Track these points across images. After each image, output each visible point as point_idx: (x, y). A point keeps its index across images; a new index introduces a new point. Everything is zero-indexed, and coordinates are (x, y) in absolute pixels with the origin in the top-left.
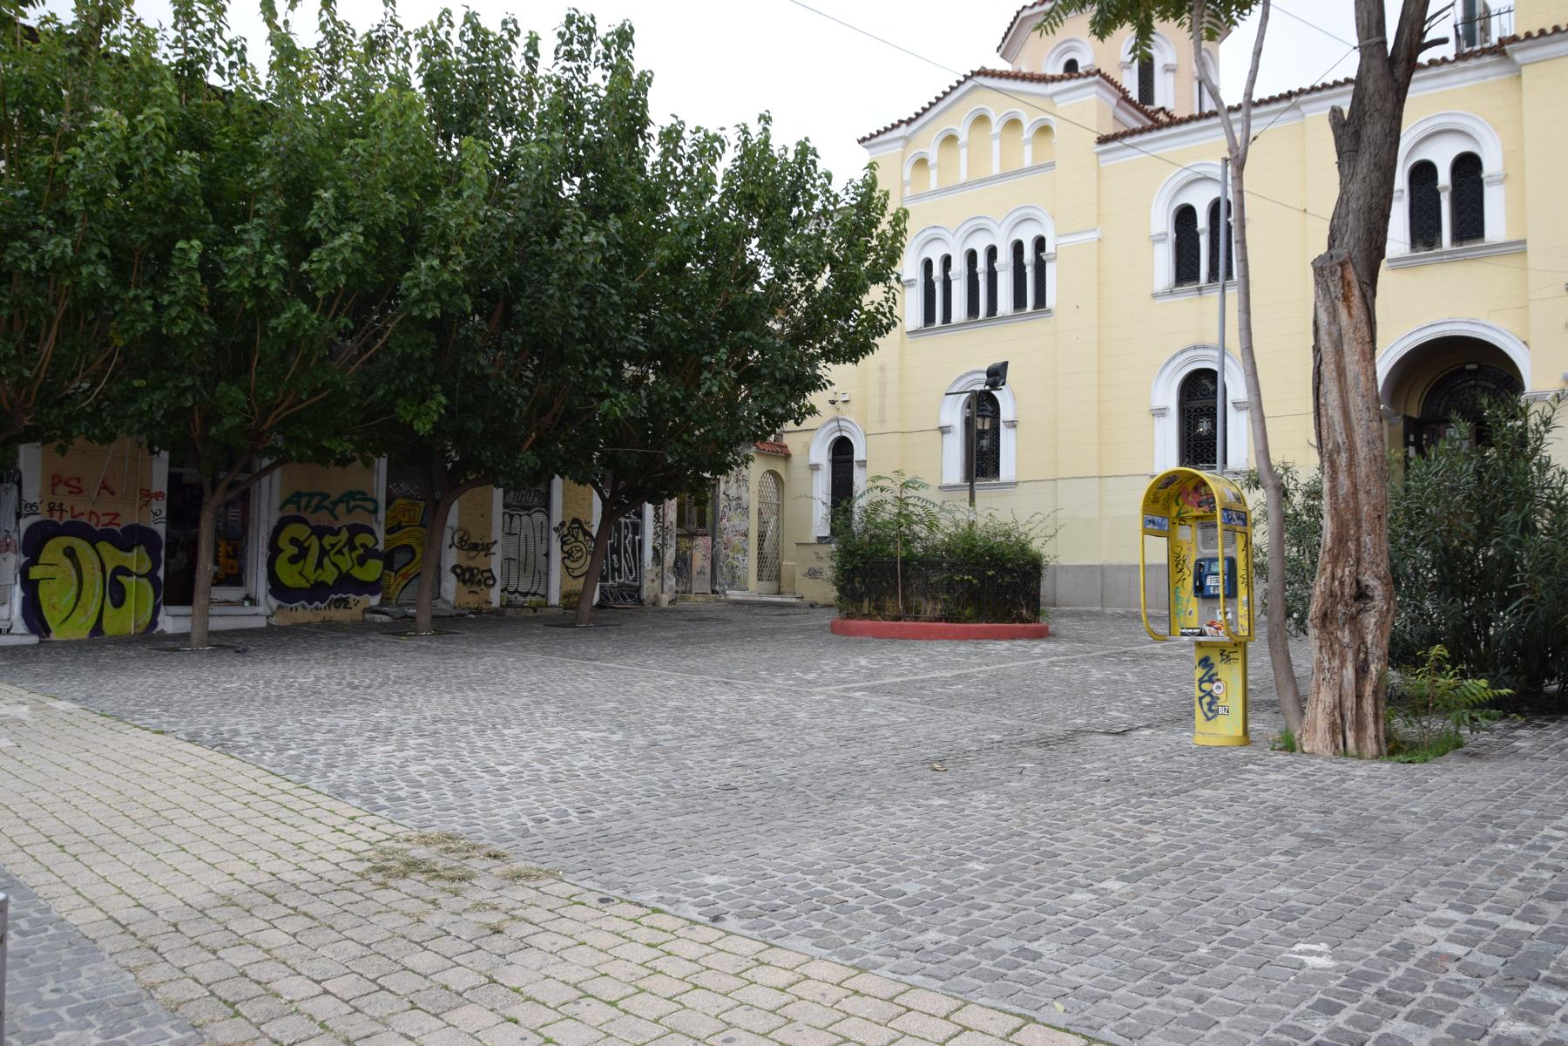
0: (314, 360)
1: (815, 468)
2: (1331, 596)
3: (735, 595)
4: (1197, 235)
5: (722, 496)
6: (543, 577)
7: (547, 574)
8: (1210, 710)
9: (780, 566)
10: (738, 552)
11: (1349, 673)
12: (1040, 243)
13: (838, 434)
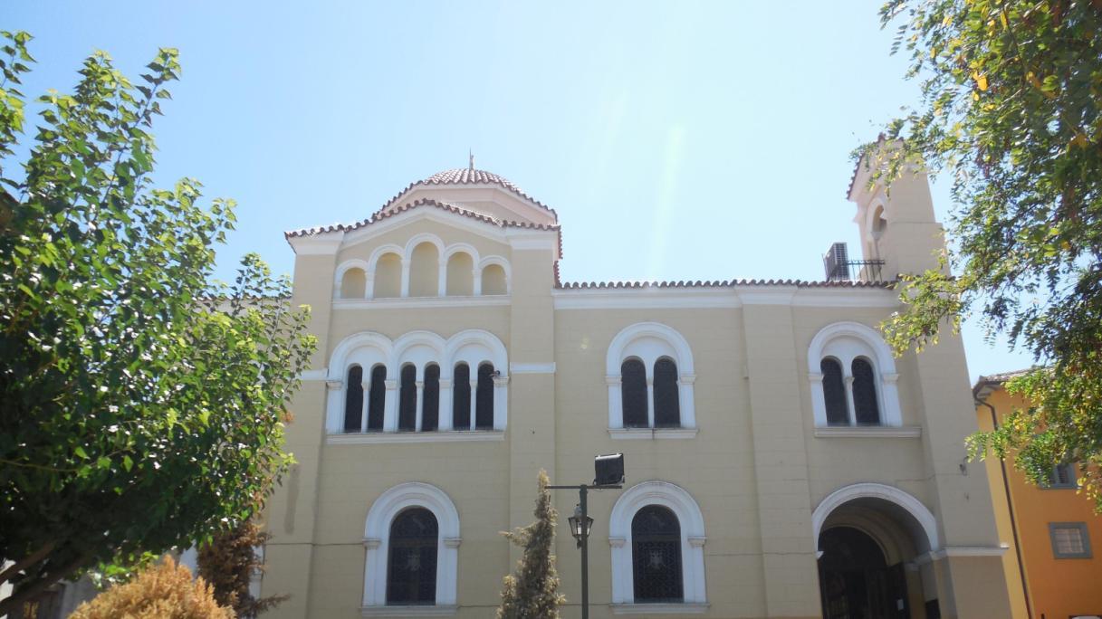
4: (645, 386)
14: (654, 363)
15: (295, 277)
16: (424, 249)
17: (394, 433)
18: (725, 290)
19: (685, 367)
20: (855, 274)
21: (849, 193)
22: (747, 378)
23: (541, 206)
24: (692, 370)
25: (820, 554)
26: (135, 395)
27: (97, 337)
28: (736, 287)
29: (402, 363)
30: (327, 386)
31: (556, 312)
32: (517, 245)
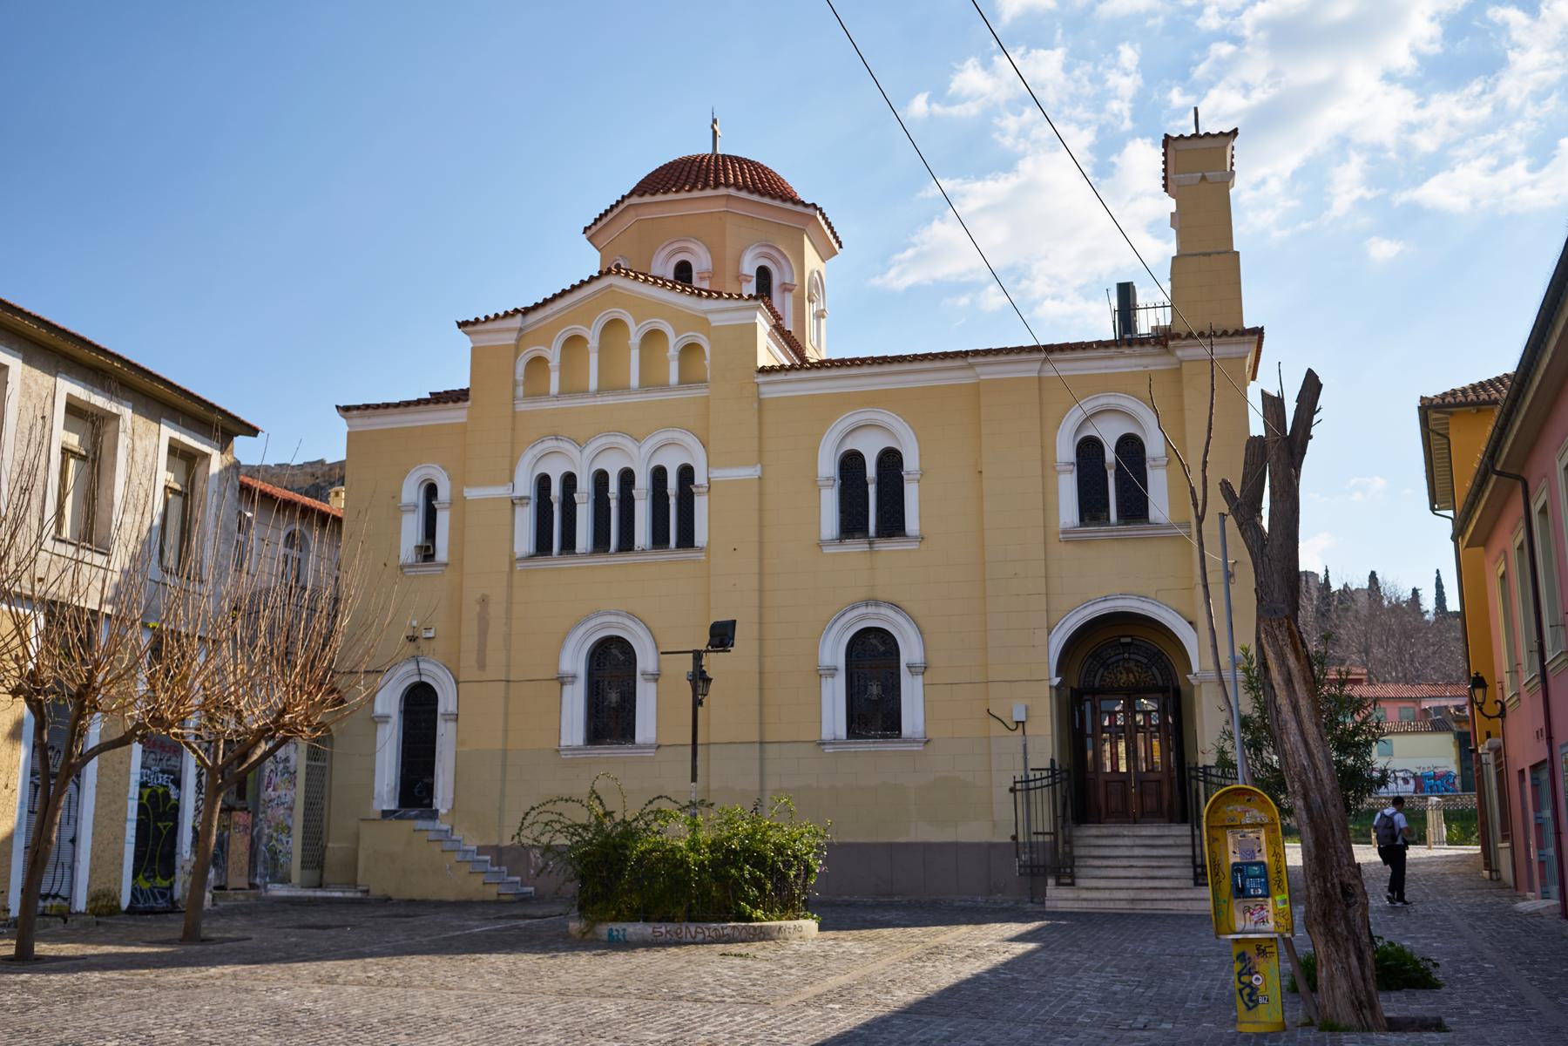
1: (385, 719)
2: (1326, 896)
3: (278, 891)
4: (866, 485)
6: (67, 871)
7: (72, 868)
8: (1251, 1000)
9: (324, 848)
11: (1354, 961)
12: (686, 473)
13: (416, 679)
14: (1115, 441)
16: (614, 325)
17: (531, 557)
19: (911, 463)
20: (1145, 323)
21: (1165, 186)
22: (981, 472)
23: (597, 278)
24: (917, 468)
25: (1056, 681)
27: (87, 467)
29: (593, 470)
32: (717, 320)
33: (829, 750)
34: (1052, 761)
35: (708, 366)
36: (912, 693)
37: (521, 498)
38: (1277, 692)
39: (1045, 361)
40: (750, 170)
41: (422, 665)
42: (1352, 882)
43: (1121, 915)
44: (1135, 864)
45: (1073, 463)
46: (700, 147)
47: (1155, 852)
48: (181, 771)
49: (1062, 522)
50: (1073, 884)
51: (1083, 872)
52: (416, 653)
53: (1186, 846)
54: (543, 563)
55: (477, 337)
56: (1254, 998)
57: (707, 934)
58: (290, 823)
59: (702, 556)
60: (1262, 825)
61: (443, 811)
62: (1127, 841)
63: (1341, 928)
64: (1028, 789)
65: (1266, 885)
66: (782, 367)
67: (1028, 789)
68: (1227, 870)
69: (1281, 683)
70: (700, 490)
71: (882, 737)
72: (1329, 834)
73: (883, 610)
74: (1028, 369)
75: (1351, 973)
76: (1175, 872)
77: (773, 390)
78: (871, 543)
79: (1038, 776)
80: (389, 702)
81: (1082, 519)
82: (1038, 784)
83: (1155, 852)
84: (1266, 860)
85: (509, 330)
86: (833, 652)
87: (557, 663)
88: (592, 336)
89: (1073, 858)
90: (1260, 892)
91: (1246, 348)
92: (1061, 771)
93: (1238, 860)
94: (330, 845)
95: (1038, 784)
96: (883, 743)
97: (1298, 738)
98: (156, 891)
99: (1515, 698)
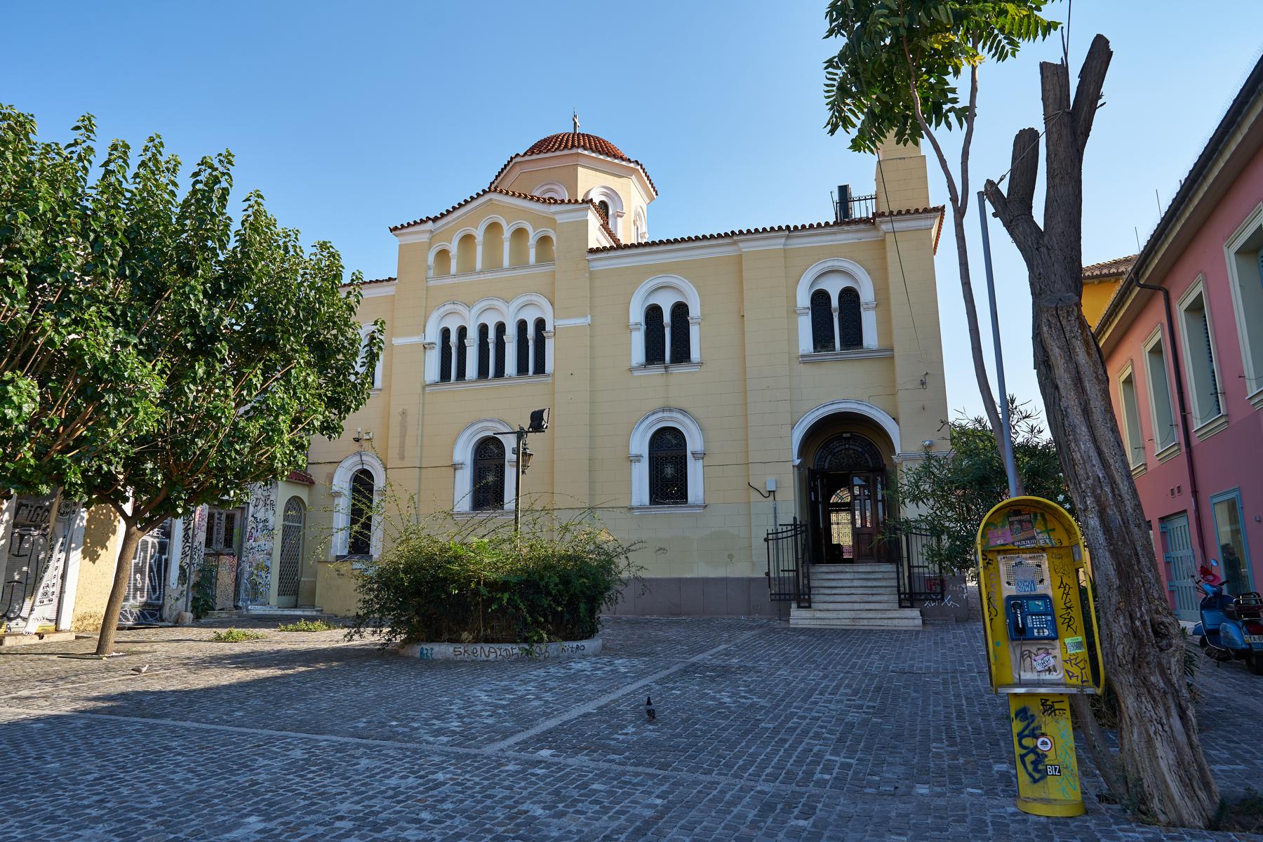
0: (41, 286)
1: (338, 494)
5: (250, 518)
8: (1036, 770)
10: (263, 569)
11: (1176, 723)
12: (540, 324)
13: (360, 467)
15: (1047, 120)
16: (494, 227)
17: (436, 384)
18: (727, 240)
19: (694, 311)
20: (859, 210)
25: (797, 462)
26: (507, 559)
28: (735, 238)
30: (425, 348)
31: (591, 272)
33: (636, 513)
34: (795, 518)
35: (555, 251)
36: (695, 471)
37: (429, 344)
38: (1063, 392)
39: (788, 237)
40: (595, 141)
41: (364, 458)
42: (1164, 620)
43: (847, 630)
44: (855, 592)
45: (808, 308)
46: (563, 127)
47: (869, 584)
48: (171, 526)
49: (801, 349)
50: (809, 607)
51: (818, 598)
52: (359, 449)
53: (892, 579)
54: (445, 387)
55: (402, 238)
56: (1040, 767)
57: (499, 653)
58: (269, 565)
59: (550, 379)
60: (1043, 549)
61: (375, 556)
62: (848, 576)
63: (1155, 679)
64: (778, 539)
65: (1053, 625)
66: (605, 248)
67: (778, 539)
68: (1000, 605)
69: (1069, 382)
70: (549, 334)
71: (674, 503)
72: (1134, 561)
73: (674, 415)
74: (778, 244)
75: (1175, 738)
76: (885, 598)
77: (602, 264)
78: (666, 368)
79: (785, 529)
80: (342, 481)
81: (815, 348)
82: (785, 535)
83: (869, 584)
84: (1050, 593)
85: (423, 232)
86: (640, 444)
87: (452, 456)
88: (479, 234)
89: (810, 588)
90: (1046, 633)
91: (928, 222)
92: (801, 526)
93: (1014, 593)
94: (302, 579)
95: (785, 535)
96: (675, 507)
97: (1090, 445)
98: (145, 612)
99: (1143, 468)
